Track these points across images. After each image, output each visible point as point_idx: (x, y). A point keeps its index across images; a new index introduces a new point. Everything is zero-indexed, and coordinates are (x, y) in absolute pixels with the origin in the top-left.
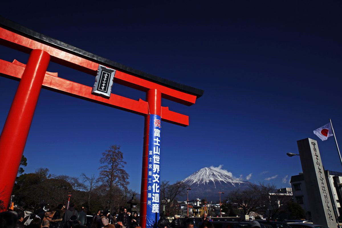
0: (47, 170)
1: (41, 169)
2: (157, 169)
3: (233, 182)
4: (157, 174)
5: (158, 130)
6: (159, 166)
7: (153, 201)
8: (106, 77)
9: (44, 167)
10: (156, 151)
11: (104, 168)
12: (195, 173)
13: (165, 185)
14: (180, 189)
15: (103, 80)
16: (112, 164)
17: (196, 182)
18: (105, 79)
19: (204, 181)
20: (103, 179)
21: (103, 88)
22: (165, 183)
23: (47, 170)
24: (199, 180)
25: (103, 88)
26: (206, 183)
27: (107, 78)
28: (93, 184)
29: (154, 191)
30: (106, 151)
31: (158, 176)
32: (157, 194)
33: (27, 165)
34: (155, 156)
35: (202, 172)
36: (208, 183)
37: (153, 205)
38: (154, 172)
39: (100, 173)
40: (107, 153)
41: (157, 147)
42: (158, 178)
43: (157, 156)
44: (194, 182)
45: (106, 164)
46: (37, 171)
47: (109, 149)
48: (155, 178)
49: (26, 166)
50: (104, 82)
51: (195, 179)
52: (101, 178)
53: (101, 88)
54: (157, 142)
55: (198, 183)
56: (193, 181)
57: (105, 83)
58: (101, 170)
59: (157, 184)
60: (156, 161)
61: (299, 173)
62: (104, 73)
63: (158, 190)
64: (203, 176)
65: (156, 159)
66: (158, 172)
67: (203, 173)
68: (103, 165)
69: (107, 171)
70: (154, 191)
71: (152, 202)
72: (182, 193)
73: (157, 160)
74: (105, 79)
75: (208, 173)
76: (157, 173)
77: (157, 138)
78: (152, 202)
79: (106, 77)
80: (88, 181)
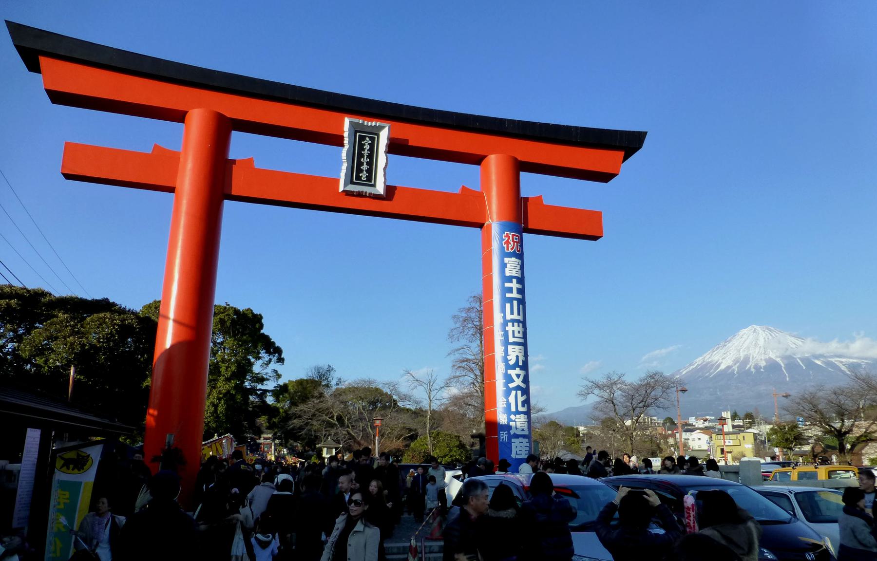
0: (330, 369)
1: (318, 369)
2: (517, 357)
3: (841, 362)
4: (518, 369)
5: (514, 259)
6: (522, 347)
7: (512, 432)
8: (367, 147)
9: (323, 363)
10: (512, 313)
11: (461, 351)
12: (722, 344)
13: (615, 383)
14: (658, 392)
15: (361, 156)
16: (479, 342)
17: (729, 367)
18: (366, 152)
19: (751, 364)
20: (461, 379)
21: (364, 175)
22: (615, 378)
23: (330, 369)
24: (736, 361)
25: (364, 175)
26: (757, 367)
27: (371, 149)
28: (433, 393)
29: (513, 409)
30: (461, 311)
31: (522, 373)
32: (522, 415)
33: (285, 362)
34: (510, 324)
35: (743, 339)
36: (765, 367)
37: (513, 440)
38: (512, 363)
39: (454, 366)
40: (464, 315)
41: (515, 302)
42: (521, 378)
43: (516, 324)
44: (722, 367)
45: (463, 342)
46: (310, 374)
47: (467, 305)
48: (515, 378)
49: (283, 363)
50: (365, 160)
51: (725, 357)
52: (455, 377)
53: (359, 178)
54: (515, 291)
55: (734, 370)
56: (719, 366)
57: (362, 171)
58: (452, 357)
59: (519, 392)
60: (514, 337)
61: (156, 147)
62: (362, 138)
63: (523, 406)
64: (748, 348)
65: (513, 332)
66: (521, 364)
67: (748, 341)
68: (456, 345)
69: (467, 360)
70: (513, 409)
71: (509, 433)
72: (662, 400)
73: (516, 335)
74: (366, 152)
75: (761, 342)
76: (519, 366)
77: (514, 281)
78: (509, 433)
79: (367, 147)
80: (421, 388)
